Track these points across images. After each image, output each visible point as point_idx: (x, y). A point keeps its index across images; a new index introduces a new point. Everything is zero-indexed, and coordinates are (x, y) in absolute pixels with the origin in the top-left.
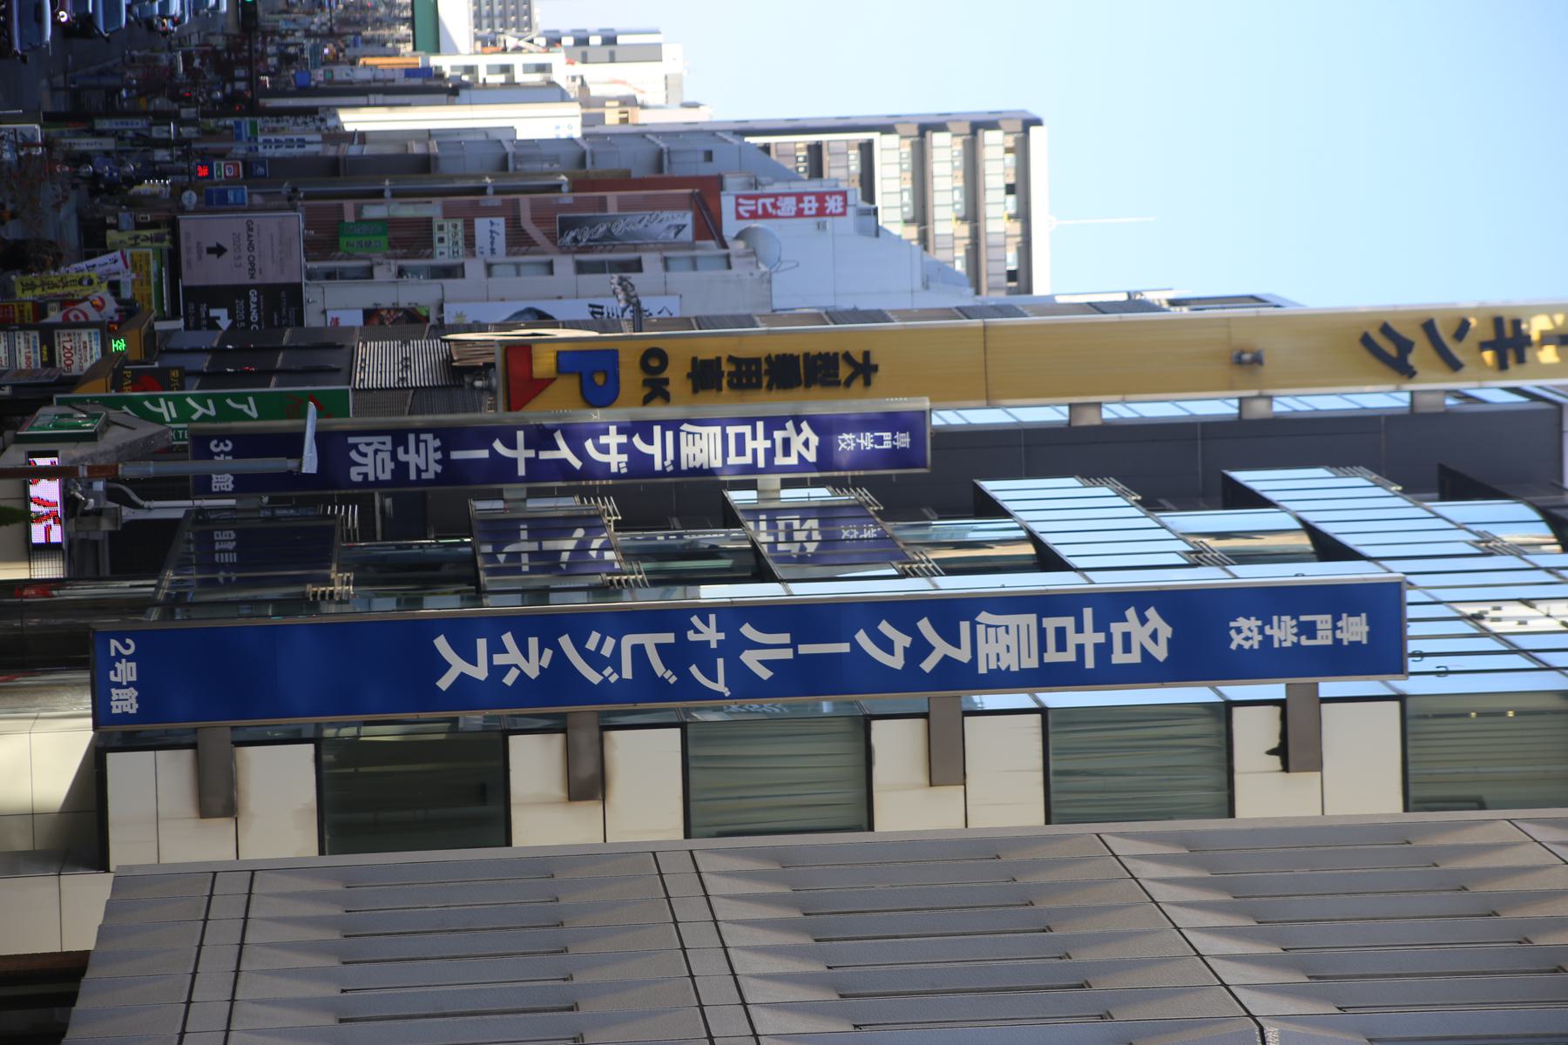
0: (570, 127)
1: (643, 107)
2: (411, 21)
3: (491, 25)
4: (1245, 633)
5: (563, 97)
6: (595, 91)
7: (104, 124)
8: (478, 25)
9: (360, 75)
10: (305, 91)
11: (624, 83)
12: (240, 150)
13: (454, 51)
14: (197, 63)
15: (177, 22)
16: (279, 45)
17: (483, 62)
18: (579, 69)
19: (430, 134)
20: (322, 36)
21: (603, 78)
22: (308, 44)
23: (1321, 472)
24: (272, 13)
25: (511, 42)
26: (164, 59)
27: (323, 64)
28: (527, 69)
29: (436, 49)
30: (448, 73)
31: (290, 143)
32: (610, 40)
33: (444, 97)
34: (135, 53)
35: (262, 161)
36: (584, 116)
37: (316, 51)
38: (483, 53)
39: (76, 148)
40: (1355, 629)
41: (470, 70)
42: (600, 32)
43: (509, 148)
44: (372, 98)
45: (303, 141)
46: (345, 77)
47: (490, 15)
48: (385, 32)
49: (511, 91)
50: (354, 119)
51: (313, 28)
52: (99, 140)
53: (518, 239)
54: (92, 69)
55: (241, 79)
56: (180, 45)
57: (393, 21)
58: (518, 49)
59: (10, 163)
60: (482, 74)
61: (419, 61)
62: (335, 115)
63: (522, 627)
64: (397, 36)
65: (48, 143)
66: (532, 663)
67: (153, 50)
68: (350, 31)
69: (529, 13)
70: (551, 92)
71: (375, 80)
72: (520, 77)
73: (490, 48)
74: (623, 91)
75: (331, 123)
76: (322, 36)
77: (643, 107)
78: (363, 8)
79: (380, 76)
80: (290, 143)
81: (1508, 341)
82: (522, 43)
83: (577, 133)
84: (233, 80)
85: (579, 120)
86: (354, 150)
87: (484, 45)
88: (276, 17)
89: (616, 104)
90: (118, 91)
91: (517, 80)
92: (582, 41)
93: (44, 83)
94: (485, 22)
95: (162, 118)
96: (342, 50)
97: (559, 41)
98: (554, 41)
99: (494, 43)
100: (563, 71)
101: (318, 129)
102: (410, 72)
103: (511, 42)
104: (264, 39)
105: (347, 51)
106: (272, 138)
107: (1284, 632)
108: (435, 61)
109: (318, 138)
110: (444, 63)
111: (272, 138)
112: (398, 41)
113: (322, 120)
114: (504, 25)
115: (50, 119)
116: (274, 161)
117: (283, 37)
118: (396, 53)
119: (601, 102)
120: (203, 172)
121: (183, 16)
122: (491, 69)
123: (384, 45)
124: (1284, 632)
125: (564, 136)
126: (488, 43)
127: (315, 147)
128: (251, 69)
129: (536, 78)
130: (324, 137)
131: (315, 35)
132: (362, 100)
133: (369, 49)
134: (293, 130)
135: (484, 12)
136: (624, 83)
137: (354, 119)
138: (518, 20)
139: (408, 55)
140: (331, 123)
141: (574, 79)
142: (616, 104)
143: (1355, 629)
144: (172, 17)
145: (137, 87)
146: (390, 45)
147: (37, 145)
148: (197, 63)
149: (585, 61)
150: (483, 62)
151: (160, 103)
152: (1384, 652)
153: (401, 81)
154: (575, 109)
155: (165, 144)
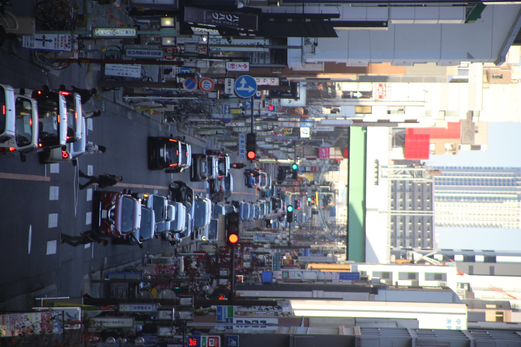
0: (458, 321)
1: (515, 310)
2: (346, 239)
3: (403, 244)
5: (454, 299)
6: (479, 295)
7: (125, 308)
8: (394, 244)
9: (308, 276)
10: (268, 286)
11: (500, 290)
12: (220, 328)
13: (376, 262)
15: (182, 235)
16: (252, 253)
17: (396, 271)
18: (466, 278)
19: (356, 321)
20: (282, 248)
21: (487, 287)
22: (273, 253)
23: (423, 325)
24: (249, 230)
25: (417, 257)
26: (171, 260)
27: (282, 267)
28: (428, 277)
29: (363, 260)
30: (371, 277)
31: (256, 324)
32: (491, 259)
33: (367, 294)
34: (152, 256)
35: (234, 337)
36: (469, 314)
37: (279, 257)
38: (397, 264)
39: (105, 325)
41: (387, 275)
42: (483, 252)
43: (413, 335)
44: (315, 293)
45: (264, 322)
46: (297, 277)
47: (403, 236)
48: (327, 246)
49: (415, 292)
50: (302, 308)
51: (277, 241)
52: (121, 320)
54: (121, 268)
55: (224, 277)
56: (183, 251)
57: (332, 238)
58: (422, 262)
59: (57, 335)
60: (395, 279)
61: (350, 267)
62: (289, 304)
64: (335, 248)
65: (86, 321)
67: (164, 255)
68: (304, 244)
69: (431, 236)
70: (445, 295)
71: (318, 280)
72: (423, 282)
73: (402, 260)
74: (499, 297)
75: (285, 310)
76: (282, 248)
77: (515, 310)
78: (313, 228)
79: (322, 277)
80: (256, 324)
82: (425, 258)
83: (464, 327)
84: (218, 277)
85: (465, 317)
86: (300, 330)
87: (398, 258)
88: (251, 233)
89: (494, 306)
90: (138, 283)
91: (420, 284)
92: (470, 258)
93: (87, 277)
94: (399, 241)
95: (167, 304)
96: (296, 258)
97: (452, 258)
98: (449, 257)
99: (405, 257)
100: (454, 279)
101: (276, 314)
102: (343, 276)
103: (417, 257)
104: (242, 249)
105: (299, 258)
106: (243, 319)
108: (361, 268)
109: (275, 321)
110: (368, 270)
111: (243, 319)
112: (336, 252)
113: (279, 308)
114: (413, 244)
115: (88, 300)
116: (243, 336)
117: (255, 247)
118: (334, 261)
119: (483, 304)
120: (193, 343)
121: (186, 231)
122: (402, 276)
123: (326, 255)
125: (454, 327)
126: (400, 256)
127: (272, 325)
128: (231, 270)
129: (435, 284)
130: (280, 320)
131: (278, 247)
132: (308, 294)
133: (315, 258)
134: (257, 313)
135: (398, 234)
136: (500, 290)
137: (302, 308)
138: (423, 241)
139: (342, 263)
140: (285, 310)
141: (462, 285)
142: (494, 306)
144: (179, 232)
145: (151, 281)
146: (330, 255)
147: (78, 323)
148: (194, 264)
149: (471, 273)
150: (396, 271)
151: (167, 294)
153: (337, 281)
154: (463, 309)
155: (167, 323)
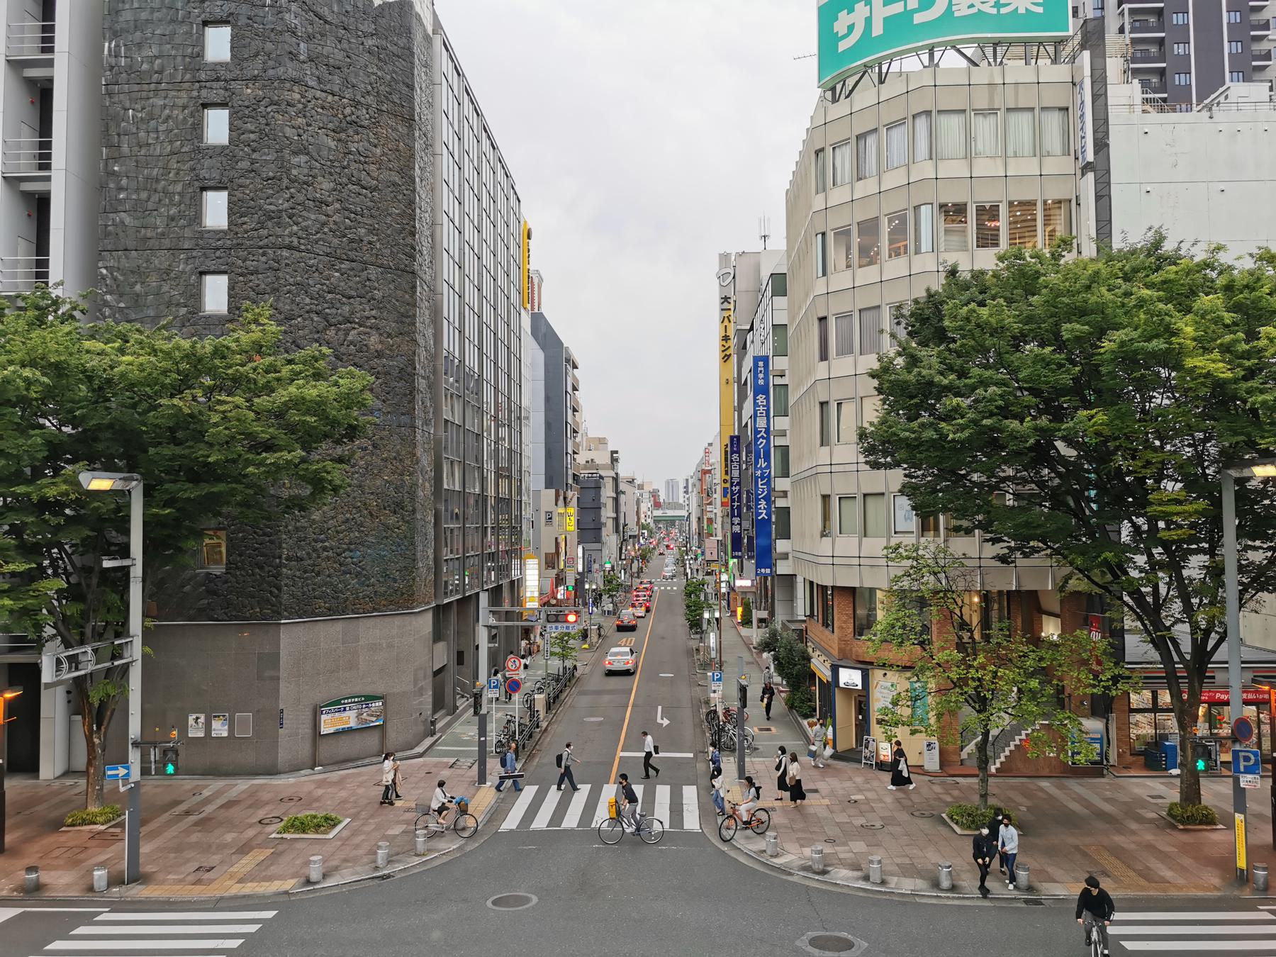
4: (761, 382)
14: (1201, 765)
40: (761, 364)
53: (710, 504)
63: (757, 504)
66: (763, 502)
81: (726, 338)
107: (761, 376)
124: (761, 376)
143: (761, 364)
148: (1201, 765)
152: (765, 359)
